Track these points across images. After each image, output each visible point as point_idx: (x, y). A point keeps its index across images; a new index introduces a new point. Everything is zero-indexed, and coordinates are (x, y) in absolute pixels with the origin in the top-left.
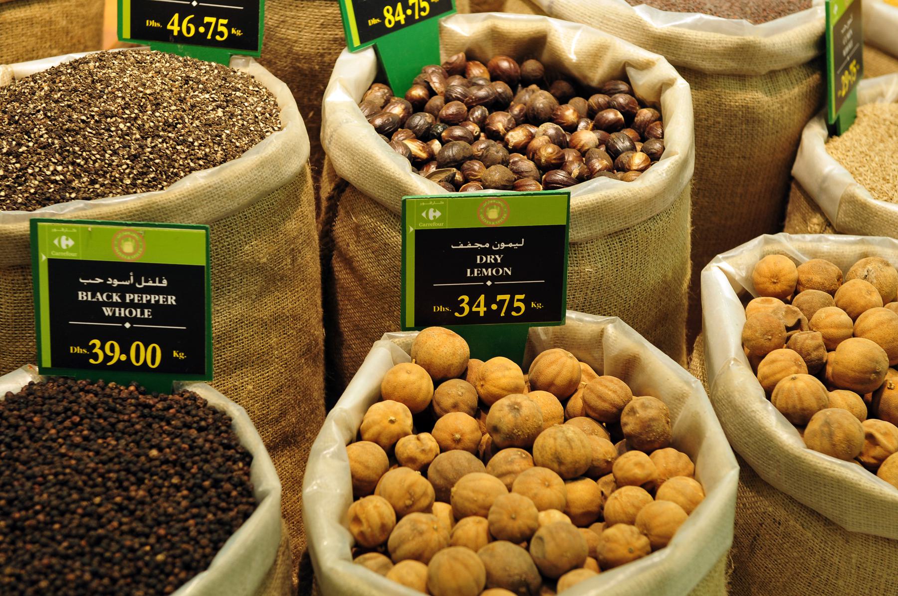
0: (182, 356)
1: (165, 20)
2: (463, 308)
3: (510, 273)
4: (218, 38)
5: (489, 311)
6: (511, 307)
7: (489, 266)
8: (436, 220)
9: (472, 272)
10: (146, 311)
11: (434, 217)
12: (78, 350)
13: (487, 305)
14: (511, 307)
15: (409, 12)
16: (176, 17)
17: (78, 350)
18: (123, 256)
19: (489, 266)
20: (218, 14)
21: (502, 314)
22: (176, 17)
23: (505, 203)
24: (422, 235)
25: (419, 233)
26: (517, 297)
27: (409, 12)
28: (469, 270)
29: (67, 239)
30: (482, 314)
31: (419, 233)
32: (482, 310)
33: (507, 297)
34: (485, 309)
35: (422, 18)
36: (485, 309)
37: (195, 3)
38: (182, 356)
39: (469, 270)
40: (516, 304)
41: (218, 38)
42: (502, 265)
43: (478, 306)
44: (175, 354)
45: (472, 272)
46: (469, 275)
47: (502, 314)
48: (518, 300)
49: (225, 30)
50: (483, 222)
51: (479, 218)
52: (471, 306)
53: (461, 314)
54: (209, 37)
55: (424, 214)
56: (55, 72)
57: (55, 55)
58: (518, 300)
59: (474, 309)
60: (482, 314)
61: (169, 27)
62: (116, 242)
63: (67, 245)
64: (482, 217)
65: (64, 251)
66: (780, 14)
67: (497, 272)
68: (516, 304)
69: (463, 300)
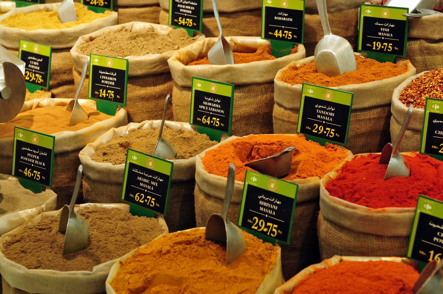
0: (397, 49)
1: (274, 32)
4: (289, 38)
7: (385, 32)
12: (435, 147)
15: (186, 22)
16: (277, 31)
17: (435, 147)
19: (385, 32)
20: (289, 30)
22: (277, 31)
27: (186, 22)
37: (283, 27)
38: (397, 49)
41: (289, 38)
42: (319, 114)
44: (395, 48)
54: (286, 37)
55: (433, 106)
61: (275, 34)
66: (19, 290)
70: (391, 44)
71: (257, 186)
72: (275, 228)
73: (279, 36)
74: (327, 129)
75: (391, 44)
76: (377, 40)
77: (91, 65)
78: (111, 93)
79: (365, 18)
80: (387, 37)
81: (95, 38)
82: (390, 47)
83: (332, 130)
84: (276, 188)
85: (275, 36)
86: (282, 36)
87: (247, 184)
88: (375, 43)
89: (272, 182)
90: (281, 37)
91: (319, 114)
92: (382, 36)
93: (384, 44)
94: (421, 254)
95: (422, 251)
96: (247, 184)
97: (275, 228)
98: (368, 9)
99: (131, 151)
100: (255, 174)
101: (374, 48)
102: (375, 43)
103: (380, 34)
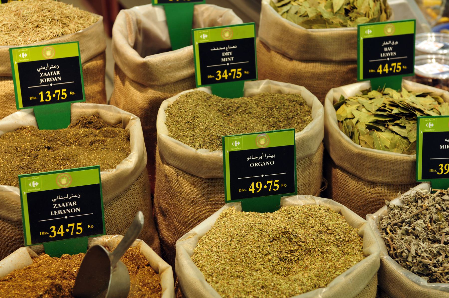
0: (73, 93)
1: (376, 68)
2: (53, 233)
3: (79, 210)
5: (66, 233)
6: (75, 230)
7: (227, 57)
8: (36, 187)
9: (53, 213)
10: (55, 212)
11: (35, 185)
13: (64, 230)
14: (75, 230)
16: (381, 66)
18: (62, 186)
19: (227, 57)
21: (72, 234)
22: (381, 66)
23: (267, 136)
24: (232, 154)
25: (231, 153)
26: (78, 224)
28: (52, 212)
29: (35, 183)
30: (62, 235)
31: (231, 153)
32: (62, 233)
33: (73, 225)
34: (64, 232)
35: (236, 79)
36: (64, 232)
38: (73, 93)
39: (52, 212)
40: (78, 228)
42: (75, 207)
43: (60, 231)
44: (89, 226)
45: (53, 213)
46: (52, 214)
47: (72, 234)
48: (79, 226)
49: (400, 67)
50: (258, 146)
51: (57, 184)
52: (57, 232)
53: (53, 236)
56: (178, 102)
57: (3, 118)
58: (79, 226)
59: (58, 233)
60: (62, 235)
61: (378, 71)
62: (70, 179)
63: (35, 185)
64: (59, 184)
65: (236, 147)
67: (73, 210)
68: (78, 228)
69: (52, 229)
70: (65, 90)
73: (384, 73)
74: (69, 225)
75: (65, 90)
76: (44, 90)
80: (55, 82)
81: (373, 115)
82: (238, 73)
85: (379, 73)
86: (389, 71)
88: (41, 93)
90: (387, 72)
91: (75, 207)
92: (226, 62)
93: (69, 225)
98: (203, 33)
99: (363, 27)
103: (223, 60)
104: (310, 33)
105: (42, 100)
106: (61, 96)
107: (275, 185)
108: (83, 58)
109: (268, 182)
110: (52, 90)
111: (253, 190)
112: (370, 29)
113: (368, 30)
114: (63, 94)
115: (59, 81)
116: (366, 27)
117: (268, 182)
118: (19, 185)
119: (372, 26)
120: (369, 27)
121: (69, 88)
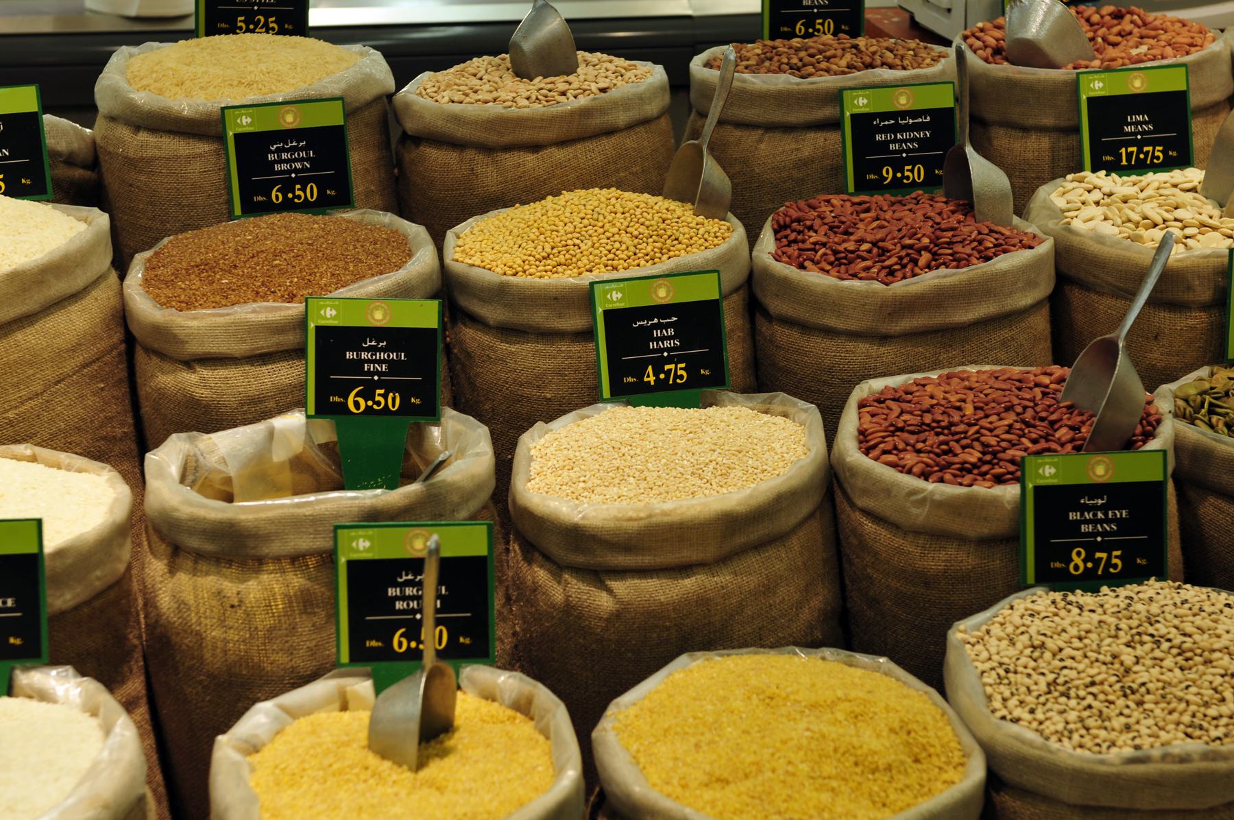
0: (1175, 154)
71: (1061, 483)
72: (1116, 557)
74: (1146, 149)
76: (1127, 144)
77: (312, 326)
78: (680, 370)
79: (1091, 100)
83: (680, 366)
84: (1110, 473)
87: (1030, 486)
88: (1123, 150)
89: (1098, 462)
92: (1135, 134)
93: (1146, 149)
94: (372, 648)
95: (371, 639)
96: (1030, 486)
97: (1116, 557)
99: (346, 531)
100: (1047, 460)
101: (1124, 163)
102: (1123, 150)
103: (1127, 129)
104: (201, 393)
105: (1124, 163)
106: (1153, 157)
107: (680, 372)
108: (1195, 100)
109: (667, 367)
110: (1140, 145)
111: (652, 379)
112: (366, 537)
113: (361, 540)
114: (1157, 154)
115: (1149, 132)
116: (353, 533)
117: (667, 367)
118: (1021, 480)
119: (370, 532)
120: (361, 532)
121: (1167, 145)
